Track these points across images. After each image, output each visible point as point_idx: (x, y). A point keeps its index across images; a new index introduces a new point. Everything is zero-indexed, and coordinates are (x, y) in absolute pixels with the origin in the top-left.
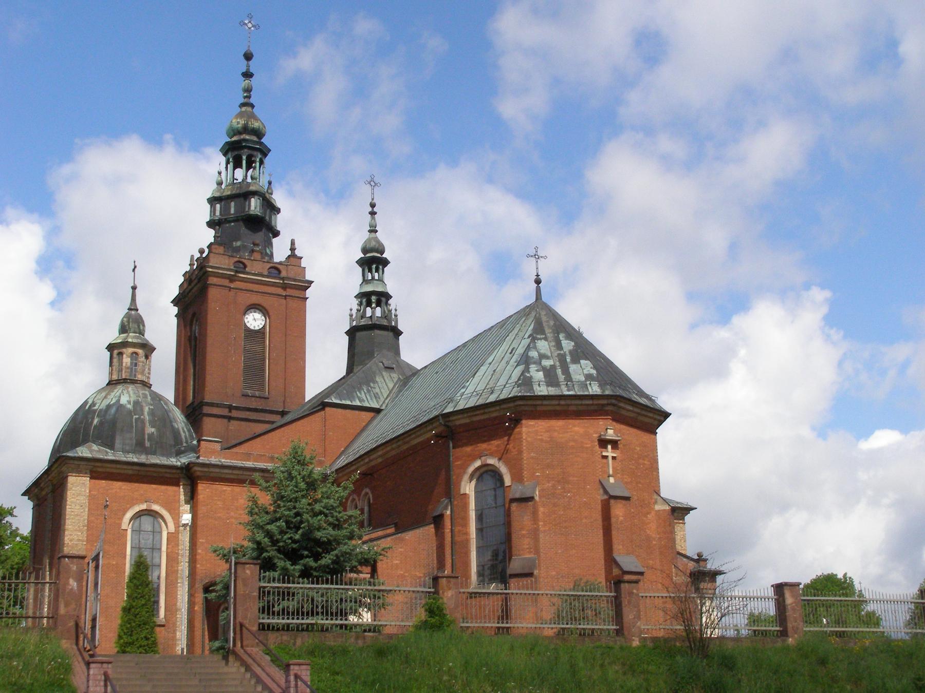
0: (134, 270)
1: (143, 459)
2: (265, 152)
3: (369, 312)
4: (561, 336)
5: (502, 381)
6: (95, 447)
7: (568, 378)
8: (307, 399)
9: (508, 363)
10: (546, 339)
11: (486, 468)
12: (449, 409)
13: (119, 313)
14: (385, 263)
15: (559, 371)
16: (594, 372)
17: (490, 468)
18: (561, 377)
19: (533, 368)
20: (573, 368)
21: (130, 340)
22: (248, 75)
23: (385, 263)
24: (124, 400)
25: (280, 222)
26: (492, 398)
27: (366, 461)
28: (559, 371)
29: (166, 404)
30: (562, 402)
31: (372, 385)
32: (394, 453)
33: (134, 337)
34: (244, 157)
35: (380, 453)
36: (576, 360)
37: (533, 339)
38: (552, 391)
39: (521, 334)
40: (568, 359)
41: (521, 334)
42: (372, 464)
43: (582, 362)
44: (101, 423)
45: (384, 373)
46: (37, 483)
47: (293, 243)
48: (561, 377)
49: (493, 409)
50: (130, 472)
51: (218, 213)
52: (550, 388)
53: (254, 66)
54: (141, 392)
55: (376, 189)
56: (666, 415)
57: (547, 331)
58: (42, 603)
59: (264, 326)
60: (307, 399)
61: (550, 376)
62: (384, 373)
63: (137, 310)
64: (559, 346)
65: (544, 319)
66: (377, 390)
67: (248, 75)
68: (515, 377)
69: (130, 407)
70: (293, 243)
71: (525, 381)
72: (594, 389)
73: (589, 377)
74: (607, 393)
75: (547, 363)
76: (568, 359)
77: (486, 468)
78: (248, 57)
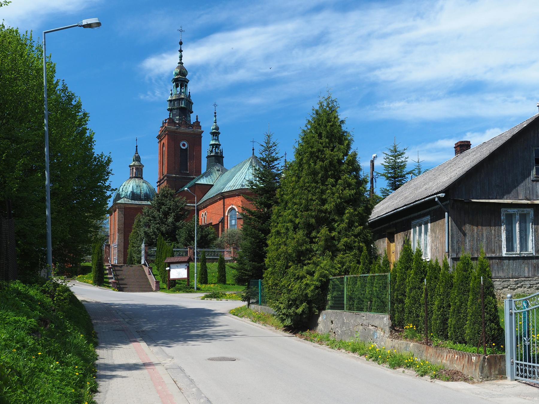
2: (187, 81)
14: (219, 133)
23: (219, 133)
47: (197, 117)
70: (197, 117)
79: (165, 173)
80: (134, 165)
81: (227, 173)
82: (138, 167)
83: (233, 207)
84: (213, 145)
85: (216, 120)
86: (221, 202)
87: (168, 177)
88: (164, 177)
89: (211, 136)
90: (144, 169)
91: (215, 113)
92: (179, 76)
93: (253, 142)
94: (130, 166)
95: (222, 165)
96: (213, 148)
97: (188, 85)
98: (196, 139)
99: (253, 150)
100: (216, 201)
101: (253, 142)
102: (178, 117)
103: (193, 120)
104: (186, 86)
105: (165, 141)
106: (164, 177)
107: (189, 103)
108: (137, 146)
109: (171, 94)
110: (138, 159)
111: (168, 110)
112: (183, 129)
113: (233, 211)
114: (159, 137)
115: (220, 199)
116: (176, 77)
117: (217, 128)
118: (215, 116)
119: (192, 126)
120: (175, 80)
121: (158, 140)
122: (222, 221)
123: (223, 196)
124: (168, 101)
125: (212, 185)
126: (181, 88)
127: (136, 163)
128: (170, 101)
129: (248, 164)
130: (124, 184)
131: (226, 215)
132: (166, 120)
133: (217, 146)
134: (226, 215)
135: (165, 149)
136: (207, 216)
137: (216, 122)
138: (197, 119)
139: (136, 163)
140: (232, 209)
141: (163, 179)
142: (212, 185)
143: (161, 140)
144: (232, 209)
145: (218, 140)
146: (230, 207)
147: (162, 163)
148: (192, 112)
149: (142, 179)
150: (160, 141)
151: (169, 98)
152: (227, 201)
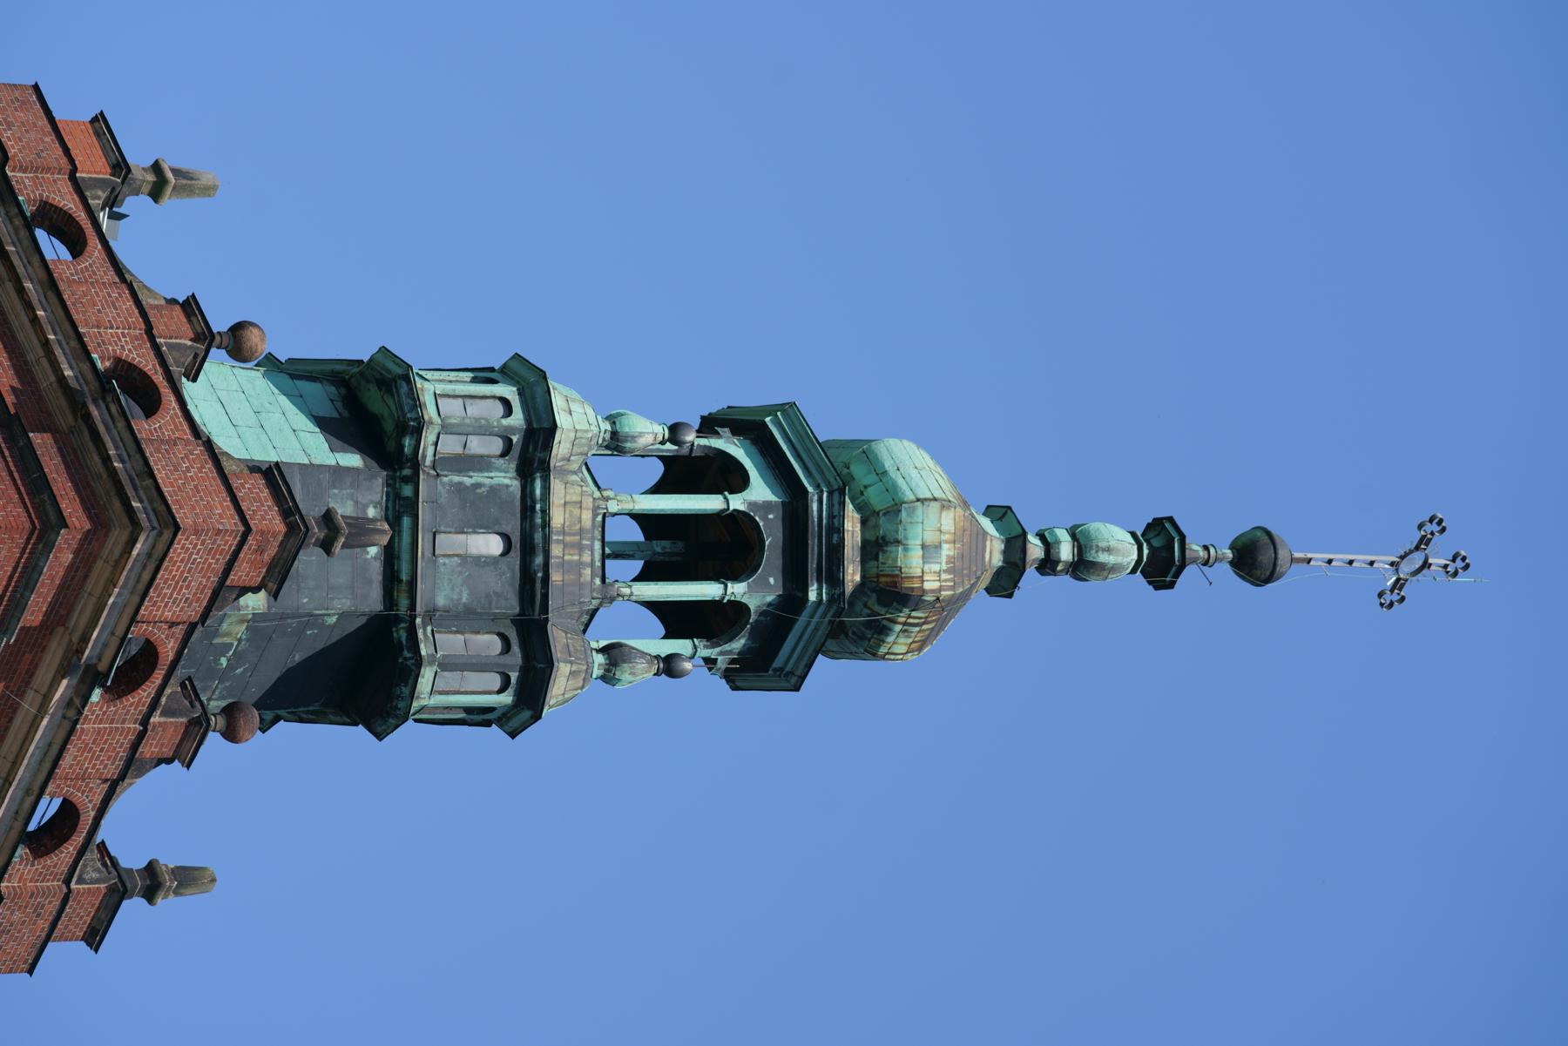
34: (737, 590)
47: (189, 878)
51: (450, 446)
53: (1208, 587)
70: (189, 878)
78: (1254, 559)
151: (575, 419)
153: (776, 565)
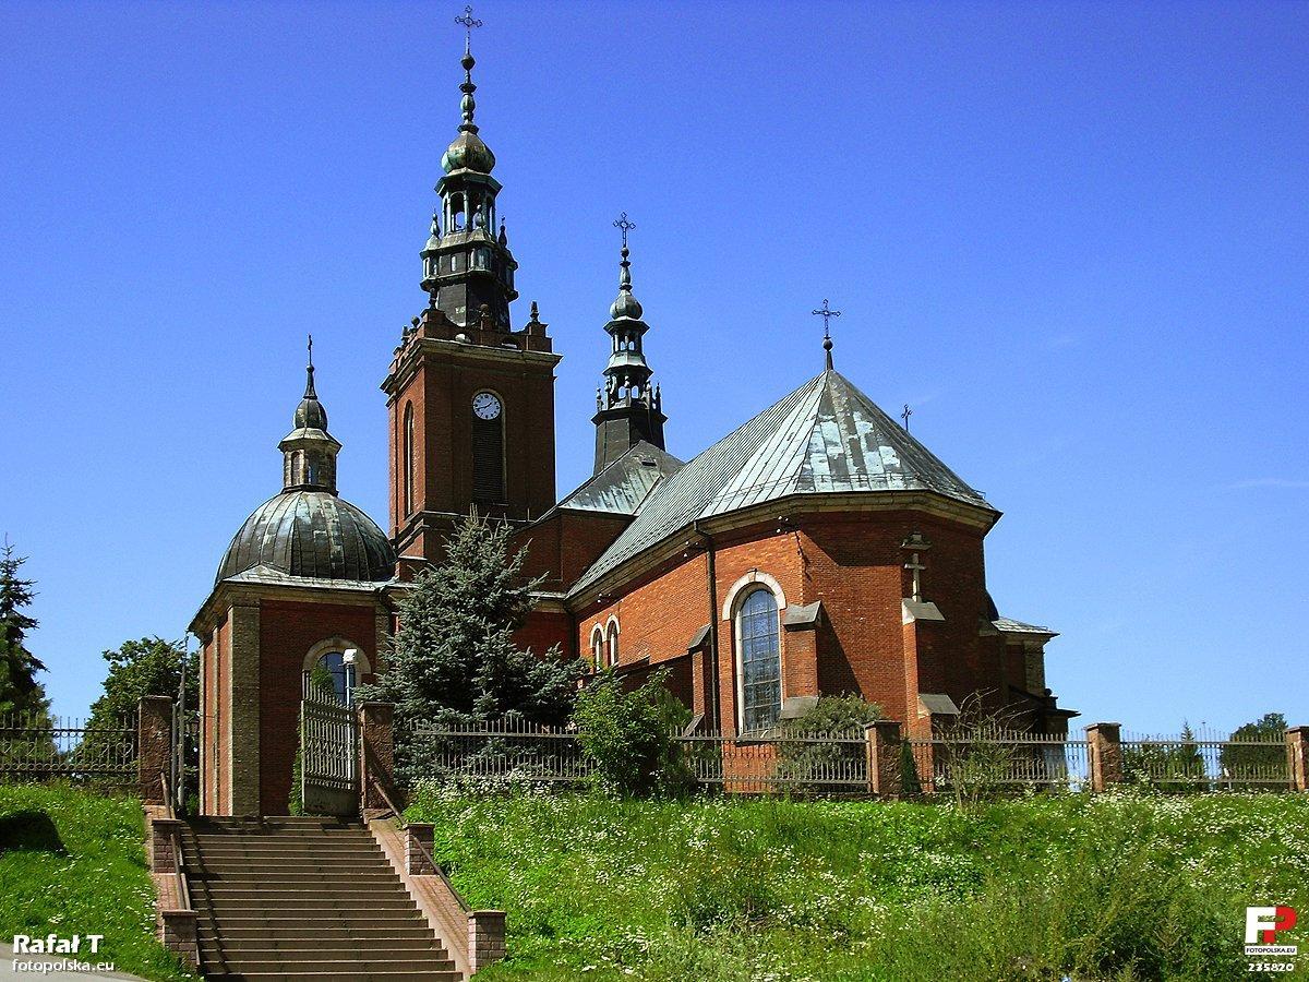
0: (309, 348)
1: (326, 583)
2: (494, 189)
3: (622, 392)
4: (857, 416)
5: (776, 476)
6: (266, 571)
7: (862, 470)
8: (939, 617)
9: (783, 453)
10: (835, 420)
11: (753, 588)
12: (707, 513)
13: (297, 404)
14: (643, 328)
15: (850, 461)
16: (897, 462)
17: (760, 586)
18: (853, 469)
19: (815, 457)
20: (868, 456)
21: (307, 436)
22: (469, 88)
23: (643, 328)
24: (301, 512)
25: (520, 281)
26: (760, 499)
27: (611, 581)
28: (850, 461)
29: (356, 515)
30: (852, 502)
31: (623, 485)
32: (643, 570)
33: (311, 433)
35: (627, 571)
36: (872, 447)
37: (818, 421)
38: (840, 487)
39: (802, 415)
40: (863, 444)
41: (802, 415)
42: (618, 584)
43: (881, 448)
44: (274, 541)
45: (641, 471)
46: (200, 616)
47: (534, 307)
48: (853, 469)
49: (764, 512)
50: (311, 600)
52: (836, 484)
54: (324, 501)
55: (629, 232)
56: (998, 515)
57: (838, 410)
58: (297, 888)
59: (500, 415)
60: (939, 617)
61: (837, 466)
62: (641, 471)
63: (315, 398)
64: (852, 429)
65: (835, 394)
66: (631, 492)
67: (469, 88)
68: (790, 471)
69: (308, 520)
70: (534, 307)
71: (804, 477)
72: (896, 484)
73: (890, 468)
74: (912, 488)
75: (834, 451)
76: (863, 444)
77: (753, 588)
78: (469, 64)
79: (419, 506)
80: (301, 442)
81: (677, 479)
82: (318, 447)
83: (760, 578)
84: (618, 372)
85: (628, 279)
86: (699, 564)
87: (428, 519)
88: (413, 523)
89: (612, 342)
90: (341, 459)
91: (625, 254)
92: (463, 170)
93: (827, 314)
94: (284, 446)
95: (660, 444)
96: (621, 383)
97: (498, 200)
98: (531, 387)
99: (828, 346)
100: (677, 561)
101: (827, 314)
102: (463, 309)
103: (518, 320)
104: (491, 204)
105: (416, 393)
106: (413, 523)
107: (501, 262)
108: (311, 370)
109: (437, 232)
110: (315, 417)
111: (425, 286)
112: (483, 351)
113: (758, 607)
114: (393, 386)
115: (694, 551)
116: (454, 173)
117: (634, 309)
118: (625, 264)
119: (518, 338)
120: (451, 184)
121: (387, 398)
122: (708, 646)
123: (709, 537)
124: (424, 256)
125: (630, 519)
126: (472, 212)
127: (310, 434)
128: (433, 255)
129: (812, 403)
130: (259, 514)
131: (726, 615)
132: (416, 322)
133: (639, 376)
134: (726, 615)
135: (418, 425)
136: (636, 630)
137: (628, 288)
138: (535, 315)
139: (310, 434)
140: (756, 590)
141: (409, 530)
142: (630, 519)
143: (400, 394)
144: (756, 590)
145: (638, 352)
146: (744, 581)
147: (403, 472)
148: (515, 296)
149: (335, 494)
150: (396, 399)
151: (430, 246)
152: (727, 557)
153: (472, 185)
